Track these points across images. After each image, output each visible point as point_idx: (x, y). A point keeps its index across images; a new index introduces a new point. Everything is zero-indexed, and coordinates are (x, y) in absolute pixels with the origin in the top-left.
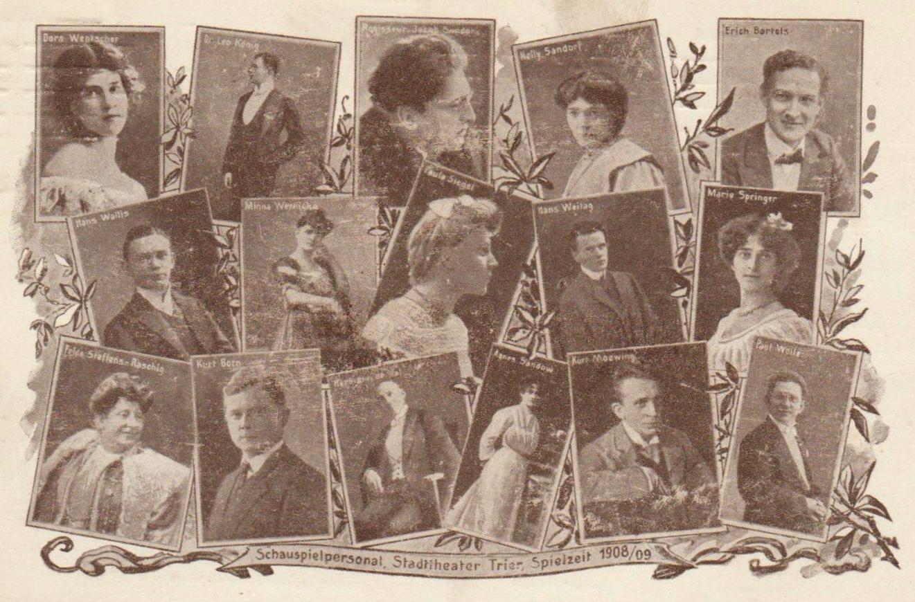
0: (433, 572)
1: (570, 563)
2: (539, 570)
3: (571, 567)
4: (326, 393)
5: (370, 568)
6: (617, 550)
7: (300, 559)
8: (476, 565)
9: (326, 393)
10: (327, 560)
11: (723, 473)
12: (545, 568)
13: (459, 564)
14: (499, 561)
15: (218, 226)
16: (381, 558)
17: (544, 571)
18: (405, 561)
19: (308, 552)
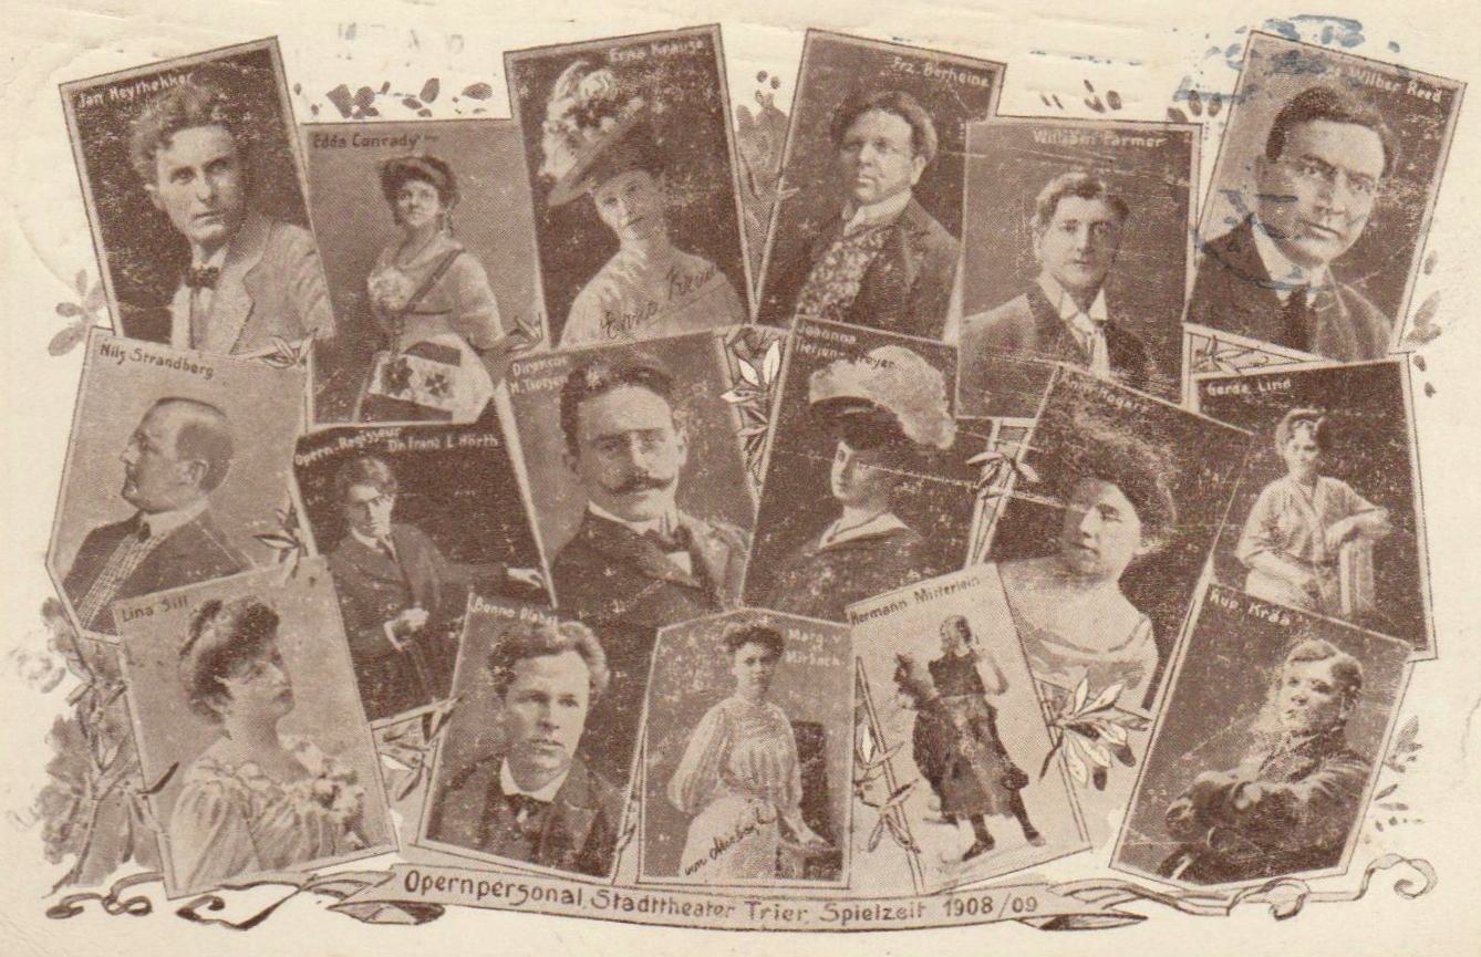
0: (665, 917)
1: (886, 918)
2: (837, 924)
3: (887, 924)
4: (810, 340)
5: (862, 923)
6: (973, 903)
7: (840, 919)
8: (800, 913)
9: (810, 340)
10: (646, 901)
11: (1301, 361)
12: (483, 898)
13: (705, 906)
14: (766, 904)
15: (1192, 334)
16: (580, 891)
17: (845, 928)
18: (617, 898)
19: (854, 910)
